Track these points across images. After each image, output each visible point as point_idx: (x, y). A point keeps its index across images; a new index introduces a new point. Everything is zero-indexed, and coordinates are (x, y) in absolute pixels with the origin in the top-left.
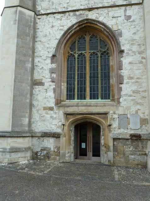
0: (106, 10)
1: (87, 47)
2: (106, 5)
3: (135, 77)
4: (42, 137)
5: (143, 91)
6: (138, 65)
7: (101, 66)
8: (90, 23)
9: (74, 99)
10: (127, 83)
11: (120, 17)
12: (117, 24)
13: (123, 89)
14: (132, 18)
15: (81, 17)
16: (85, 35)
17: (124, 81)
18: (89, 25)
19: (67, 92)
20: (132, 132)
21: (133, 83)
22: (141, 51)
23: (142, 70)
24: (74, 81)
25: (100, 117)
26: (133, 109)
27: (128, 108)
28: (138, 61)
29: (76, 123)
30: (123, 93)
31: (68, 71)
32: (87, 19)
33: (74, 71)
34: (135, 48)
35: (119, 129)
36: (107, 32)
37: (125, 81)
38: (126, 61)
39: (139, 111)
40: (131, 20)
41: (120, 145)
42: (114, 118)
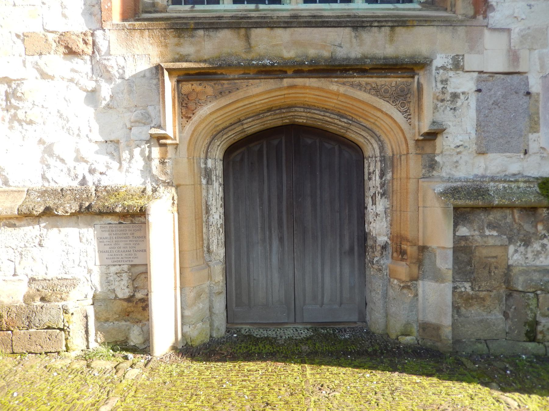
4: (26, 216)
25: (377, 91)
29: (232, 136)
35: (481, 153)
41: (486, 238)
42: (455, 96)
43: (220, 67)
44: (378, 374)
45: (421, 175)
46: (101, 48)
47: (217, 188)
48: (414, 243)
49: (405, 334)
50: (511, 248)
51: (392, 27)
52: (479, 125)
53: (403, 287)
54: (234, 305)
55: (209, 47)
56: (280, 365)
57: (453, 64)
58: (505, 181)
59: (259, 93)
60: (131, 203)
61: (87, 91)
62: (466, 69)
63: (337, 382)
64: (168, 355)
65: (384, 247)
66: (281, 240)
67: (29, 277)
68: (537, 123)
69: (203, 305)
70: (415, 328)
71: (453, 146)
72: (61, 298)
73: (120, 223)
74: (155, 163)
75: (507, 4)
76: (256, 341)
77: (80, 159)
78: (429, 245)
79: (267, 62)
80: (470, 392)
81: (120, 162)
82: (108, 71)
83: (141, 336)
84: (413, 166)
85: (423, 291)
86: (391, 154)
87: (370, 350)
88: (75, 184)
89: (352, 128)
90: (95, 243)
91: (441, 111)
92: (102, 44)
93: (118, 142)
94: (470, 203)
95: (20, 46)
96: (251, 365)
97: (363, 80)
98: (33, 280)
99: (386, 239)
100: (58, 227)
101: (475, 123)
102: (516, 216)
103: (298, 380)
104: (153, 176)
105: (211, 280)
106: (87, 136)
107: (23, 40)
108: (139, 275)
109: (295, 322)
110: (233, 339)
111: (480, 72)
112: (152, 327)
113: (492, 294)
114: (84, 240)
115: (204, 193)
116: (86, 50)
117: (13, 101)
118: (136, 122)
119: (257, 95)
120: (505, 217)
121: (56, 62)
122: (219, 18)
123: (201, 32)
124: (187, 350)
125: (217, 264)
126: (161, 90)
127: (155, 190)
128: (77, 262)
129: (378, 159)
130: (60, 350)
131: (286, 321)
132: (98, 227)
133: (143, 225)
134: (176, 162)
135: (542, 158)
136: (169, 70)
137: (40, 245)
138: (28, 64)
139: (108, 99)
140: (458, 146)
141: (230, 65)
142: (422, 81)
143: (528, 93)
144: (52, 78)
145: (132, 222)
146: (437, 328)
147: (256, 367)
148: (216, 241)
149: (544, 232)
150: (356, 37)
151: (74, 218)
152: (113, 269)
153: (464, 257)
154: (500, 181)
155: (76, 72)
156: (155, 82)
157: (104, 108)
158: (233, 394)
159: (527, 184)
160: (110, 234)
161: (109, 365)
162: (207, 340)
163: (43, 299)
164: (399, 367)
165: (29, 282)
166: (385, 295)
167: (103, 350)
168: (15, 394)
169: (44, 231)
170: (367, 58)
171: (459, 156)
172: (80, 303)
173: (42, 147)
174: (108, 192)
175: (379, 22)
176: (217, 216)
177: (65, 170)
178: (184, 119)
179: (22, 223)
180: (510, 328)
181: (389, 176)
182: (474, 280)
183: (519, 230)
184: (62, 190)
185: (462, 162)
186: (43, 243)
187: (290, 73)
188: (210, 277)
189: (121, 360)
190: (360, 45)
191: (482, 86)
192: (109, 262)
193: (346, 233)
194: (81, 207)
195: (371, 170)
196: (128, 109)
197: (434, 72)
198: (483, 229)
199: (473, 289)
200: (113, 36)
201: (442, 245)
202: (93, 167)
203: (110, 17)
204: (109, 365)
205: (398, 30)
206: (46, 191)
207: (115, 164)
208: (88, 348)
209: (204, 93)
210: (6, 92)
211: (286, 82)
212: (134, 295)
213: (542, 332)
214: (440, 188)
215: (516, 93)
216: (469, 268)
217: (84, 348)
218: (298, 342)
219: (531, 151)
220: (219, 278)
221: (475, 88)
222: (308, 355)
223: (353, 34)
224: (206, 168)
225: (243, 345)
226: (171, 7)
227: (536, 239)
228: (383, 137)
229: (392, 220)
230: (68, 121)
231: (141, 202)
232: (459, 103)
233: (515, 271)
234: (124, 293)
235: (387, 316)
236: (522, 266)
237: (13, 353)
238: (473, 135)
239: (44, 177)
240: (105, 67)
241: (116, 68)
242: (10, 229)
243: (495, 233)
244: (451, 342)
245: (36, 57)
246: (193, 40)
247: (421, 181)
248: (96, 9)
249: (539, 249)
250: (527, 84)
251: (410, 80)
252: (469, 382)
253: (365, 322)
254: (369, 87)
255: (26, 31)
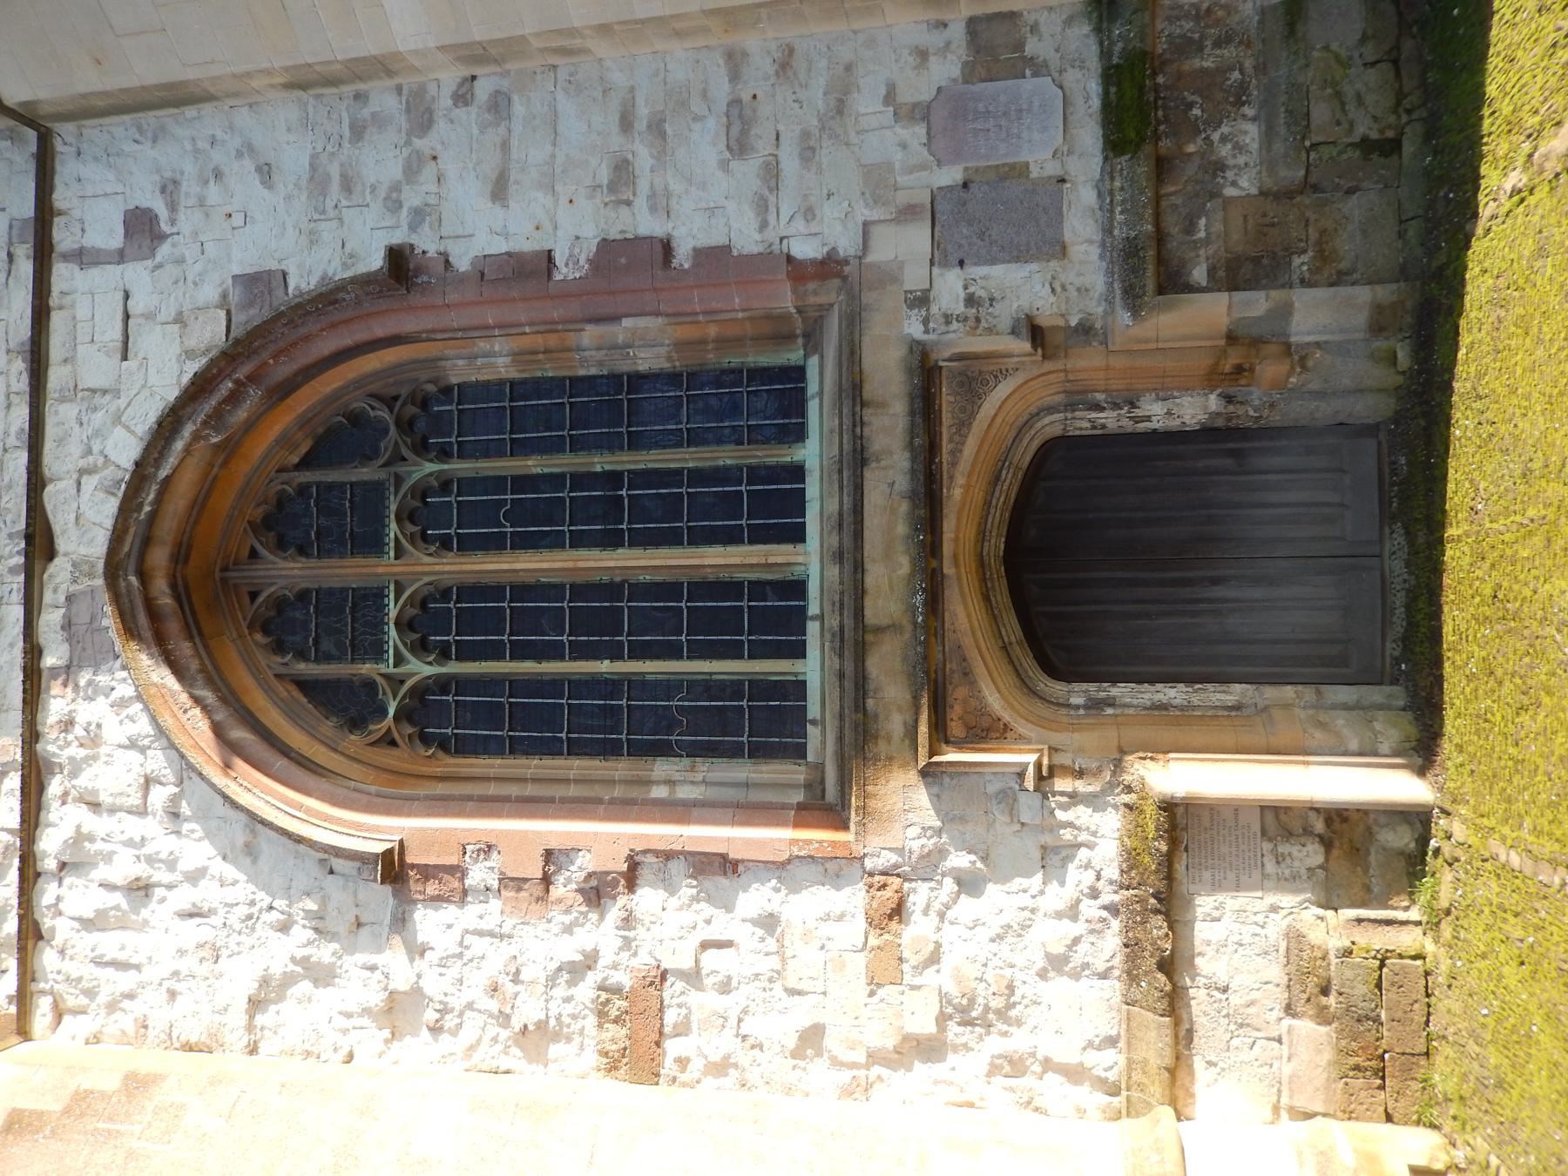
0: (58, 416)
1: (348, 571)
2: (21, 415)
3: (616, 141)
4: (1174, 1004)
5: (735, 76)
6: (517, 127)
7: (520, 448)
8: (147, 541)
9: (800, 687)
10: (661, 203)
11: (127, 296)
12: (179, 320)
13: (718, 239)
14: (145, 204)
15: (93, 618)
16: (253, 596)
17: (643, 230)
18: (159, 557)
19: (734, 752)
20: (1090, 136)
21: (661, 155)
22: (408, 110)
23: (560, 95)
24: (638, 685)
25: (963, 425)
26: (893, 143)
27: (877, 181)
28: (483, 128)
30: (747, 238)
31: (549, 749)
32: (113, 570)
33: (552, 686)
34: (381, 162)
35: (1062, 251)
36: (234, 398)
37: (647, 224)
38: (474, 228)
39: (906, 96)
40: (160, 207)
41: (1208, 239)
42: (971, 300)
43: (927, 673)
44: (1457, 415)
45: (1102, 348)
46: (893, 861)
47: (1119, 691)
48: (1223, 353)
49: (1393, 360)
50: (1230, 192)
51: (863, 405)
52: (1017, 259)
53: (1304, 367)
54: (1344, 670)
55: (892, 689)
56: (1446, 581)
57: (920, 307)
58: (1112, 211)
59: (964, 613)
60: (1152, 826)
61: (959, 893)
62: (927, 286)
63: (1467, 485)
64: (1432, 779)
65: (1229, 399)
66: (1215, 581)
67: (1282, 1015)
68: (1013, 166)
69: (1340, 720)
70: (1381, 344)
71: (1052, 299)
72: (1323, 959)
73: (1186, 849)
74: (1081, 786)
75: (826, 231)
76: (1412, 626)
77: (1072, 913)
78: (1224, 329)
79: (919, 599)
80: (1477, 270)
81: (1079, 846)
82: (929, 854)
83: (1399, 828)
84: (1086, 362)
85: (1309, 334)
86: (1062, 396)
87: (1423, 423)
88: (1116, 924)
89: (1015, 462)
90: (1220, 897)
91: (995, 322)
92: (887, 859)
93: (1044, 848)
94: (1150, 269)
95: (887, 991)
96: (1447, 629)
97: (946, 446)
98: (1289, 1010)
99: (1213, 397)
100: (1193, 957)
101: (1013, 266)
102: (1172, 189)
103: (1466, 549)
104: (1104, 792)
105: (1292, 705)
106: (1034, 897)
107: (879, 985)
108: (1280, 821)
109: (1380, 556)
110: (1395, 666)
111: (932, 263)
112: (1378, 804)
113: (1313, 217)
114: (1216, 914)
115: (1131, 711)
116: (895, 887)
117: (974, 1014)
118: (1011, 814)
119: (969, 616)
120: (1175, 207)
121: (917, 932)
122: (841, 676)
123: (870, 703)
124: (1423, 751)
125: (1261, 694)
126: (962, 769)
127: (1129, 789)
128: (1258, 930)
129: (1069, 415)
130: (1421, 970)
131: (1378, 573)
132: (1192, 888)
133: (1191, 810)
134: (1080, 751)
135: (1070, 152)
136: (932, 754)
137: (1225, 990)
138: (917, 981)
139: (973, 857)
140: (1053, 290)
141: (925, 658)
142: (947, 354)
143: (965, 185)
144: (938, 945)
145: (1186, 829)
146: (1378, 309)
147: (1451, 623)
148: (1218, 696)
149: (1199, 141)
150: (878, 461)
151: (1178, 927)
152: (1270, 867)
153: (1246, 271)
154: (1112, 219)
155: (928, 906)
156: (946, 780)
157: (987, 866)
158: (1484, 653)
159: (1117, 175)
160: (1206, 868)
161: (1447, 876)
162: (1409, 715)
163: (1325, 991)
164: (1446, 377)
165: (1294, 1016)
166: (1320, 395)
167: (1423, 898)
168: (1485, 1011)
169: (1201, 981)
170: (911, 443)
171: (1068, 287)
172: (1329, 929)
173: (1051, 974)
174: (1131, 868)
175: (854, 426)
176: (1172, 693)
177: (1092, 938)
178: (1008, 735)
179: (1185, 1016)
180: (1377, 182)
181: (1100, 397)
182: (1286, 250)
183: (1197, 182)
184: (1126, 946)
185: (1078, 282)
186: (1221, 984)
187: (934, 564)
188: (1287, 706)
189: (1440, 860)
190: (891, 453)
191: (954, 259)
192: (1257, 874)
193: (1201, 464)
194: (1157, 912)
195: (1088, 425)
196: (990, 825)
197: (932, 337)
198: (1195, 242)
199: (1304, 251)
200: (874, 842)
201: (1224, 310)
202: (1086, 891)
203: (846, 844)
204: (1447, 876)
205: (866, 395)
206: (1129, 973)
207: (1083, 853)
208: (1418, 923)
209: (965, 701)
210: (959, 1024)
211: (948, 569)
212: (1319, 836)
213: (1382, 132)
214: (1124, 317)
215: (964, 204)
216: (1265, 261)
217: (1419, 930)
218: (1414, 551)
219: (1059, 172)
220: (1289, 692)
221: (957, 270)
222: (1432, 533)
223: (874, 465)
224: (1086, 707)
225: (1418, 649)
226: (810, 758)
227: (1212, 152)
228: (1033, 409)
229: (1179, 389)
230: (1009, 927)
231: (1150, 809)
232: (983, 293)
233: (1269, 183)
234: (1316, 853)
235: (1361, 391)
236: (1260, 172)
237: (1427, 1054)
238: (1034, 266)
239: (1104, 976)
240: (922, 857)
241: (924, 841)
242: (1196, 1040)
243: (1203, 221)
244: (1402, 284)
245: (906, 967)
246: (881, 717)
247: (1111, 348)
248: (830, 866)
249: (1229, 146)
250: (950, 188)
251: (944, 373)
252: (1466, 268)
253: (1377, 425)
254: (957, 438)
255: (863, 980)
